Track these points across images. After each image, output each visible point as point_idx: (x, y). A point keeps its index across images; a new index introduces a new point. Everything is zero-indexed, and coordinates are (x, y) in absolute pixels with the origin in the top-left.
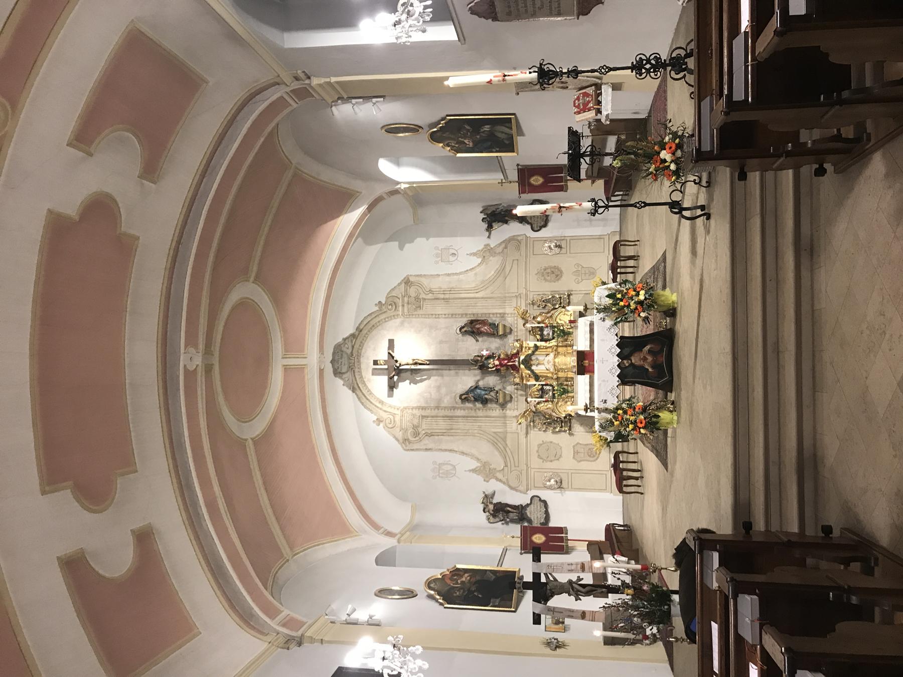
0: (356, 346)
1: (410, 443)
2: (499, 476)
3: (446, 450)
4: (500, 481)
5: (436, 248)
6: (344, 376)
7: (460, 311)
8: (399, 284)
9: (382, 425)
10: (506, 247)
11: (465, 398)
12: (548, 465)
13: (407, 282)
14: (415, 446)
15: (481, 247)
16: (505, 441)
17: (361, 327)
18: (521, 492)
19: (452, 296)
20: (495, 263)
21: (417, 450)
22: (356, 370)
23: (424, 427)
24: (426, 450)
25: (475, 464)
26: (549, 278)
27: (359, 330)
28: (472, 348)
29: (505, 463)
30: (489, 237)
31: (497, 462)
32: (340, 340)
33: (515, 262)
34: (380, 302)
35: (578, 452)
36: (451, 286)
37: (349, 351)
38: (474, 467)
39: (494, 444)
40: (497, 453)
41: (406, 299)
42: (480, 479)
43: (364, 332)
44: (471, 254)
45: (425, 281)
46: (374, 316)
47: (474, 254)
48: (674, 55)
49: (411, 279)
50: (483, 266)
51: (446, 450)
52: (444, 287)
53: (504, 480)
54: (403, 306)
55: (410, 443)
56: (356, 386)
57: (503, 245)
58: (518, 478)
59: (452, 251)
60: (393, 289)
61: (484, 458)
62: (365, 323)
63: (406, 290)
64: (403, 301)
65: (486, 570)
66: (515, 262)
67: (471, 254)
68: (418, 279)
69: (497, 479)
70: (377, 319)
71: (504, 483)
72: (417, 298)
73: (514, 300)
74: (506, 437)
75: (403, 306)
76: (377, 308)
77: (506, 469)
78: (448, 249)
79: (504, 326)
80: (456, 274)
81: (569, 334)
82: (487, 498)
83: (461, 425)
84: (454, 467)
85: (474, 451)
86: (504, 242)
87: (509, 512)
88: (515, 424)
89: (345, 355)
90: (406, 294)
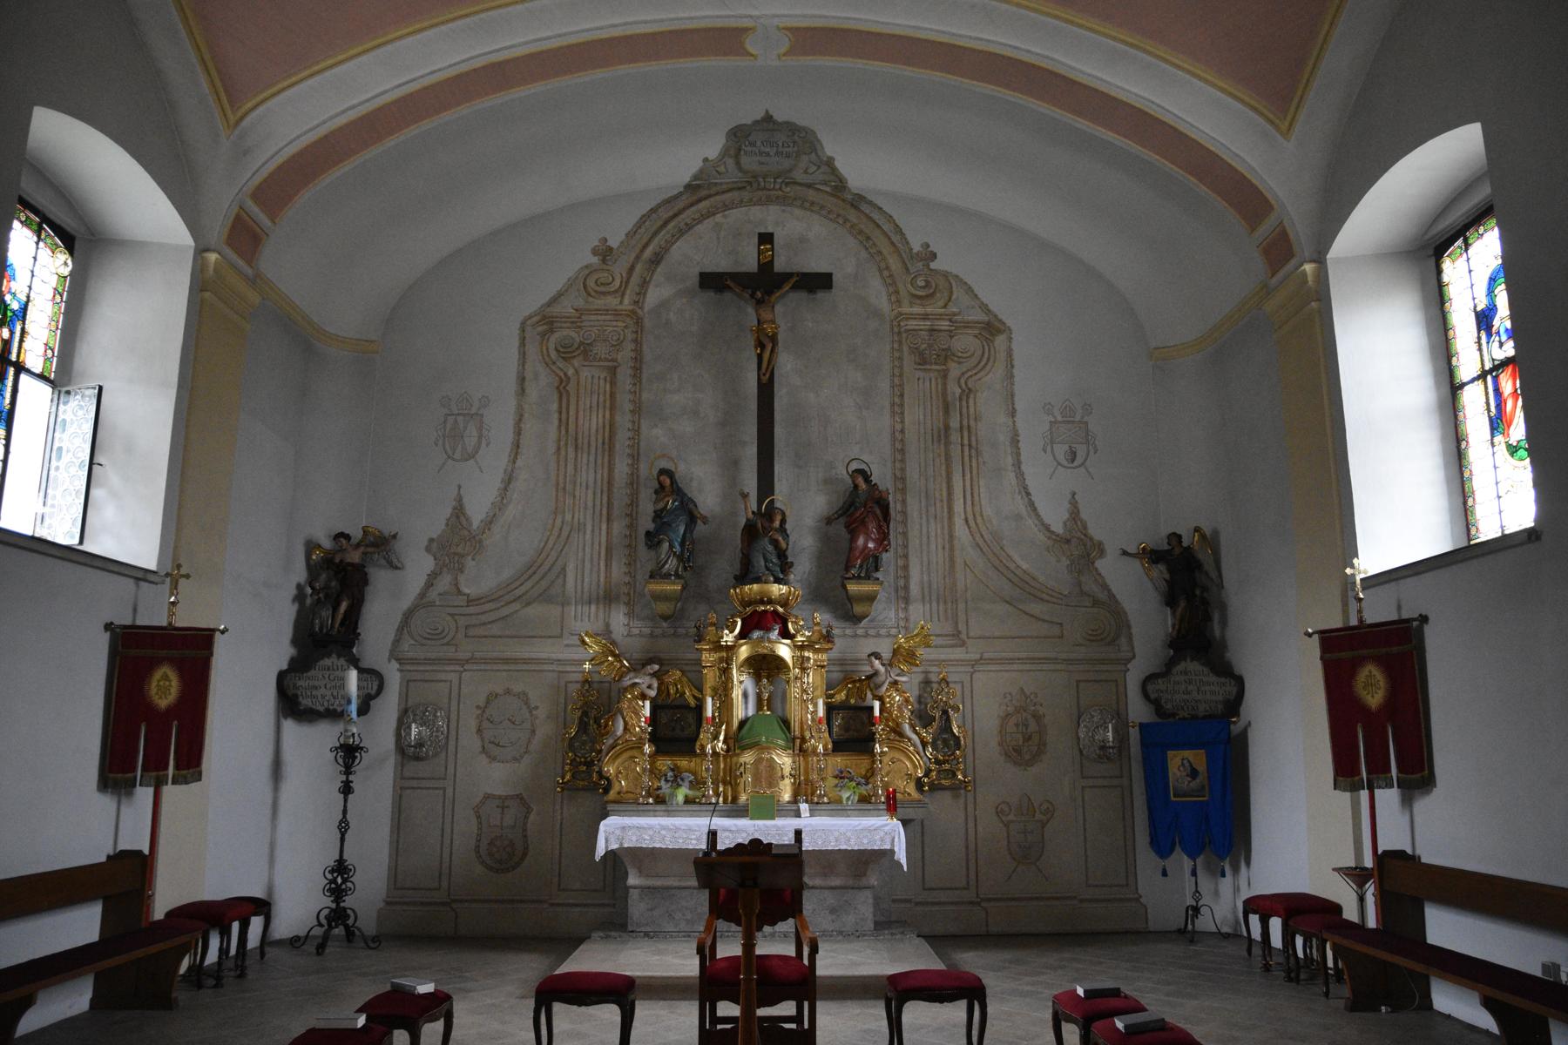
33: (1056, 630)
50: (1041, 537)
57: (1102, 596)
67: (1074, 504)
86: (1112, 596)
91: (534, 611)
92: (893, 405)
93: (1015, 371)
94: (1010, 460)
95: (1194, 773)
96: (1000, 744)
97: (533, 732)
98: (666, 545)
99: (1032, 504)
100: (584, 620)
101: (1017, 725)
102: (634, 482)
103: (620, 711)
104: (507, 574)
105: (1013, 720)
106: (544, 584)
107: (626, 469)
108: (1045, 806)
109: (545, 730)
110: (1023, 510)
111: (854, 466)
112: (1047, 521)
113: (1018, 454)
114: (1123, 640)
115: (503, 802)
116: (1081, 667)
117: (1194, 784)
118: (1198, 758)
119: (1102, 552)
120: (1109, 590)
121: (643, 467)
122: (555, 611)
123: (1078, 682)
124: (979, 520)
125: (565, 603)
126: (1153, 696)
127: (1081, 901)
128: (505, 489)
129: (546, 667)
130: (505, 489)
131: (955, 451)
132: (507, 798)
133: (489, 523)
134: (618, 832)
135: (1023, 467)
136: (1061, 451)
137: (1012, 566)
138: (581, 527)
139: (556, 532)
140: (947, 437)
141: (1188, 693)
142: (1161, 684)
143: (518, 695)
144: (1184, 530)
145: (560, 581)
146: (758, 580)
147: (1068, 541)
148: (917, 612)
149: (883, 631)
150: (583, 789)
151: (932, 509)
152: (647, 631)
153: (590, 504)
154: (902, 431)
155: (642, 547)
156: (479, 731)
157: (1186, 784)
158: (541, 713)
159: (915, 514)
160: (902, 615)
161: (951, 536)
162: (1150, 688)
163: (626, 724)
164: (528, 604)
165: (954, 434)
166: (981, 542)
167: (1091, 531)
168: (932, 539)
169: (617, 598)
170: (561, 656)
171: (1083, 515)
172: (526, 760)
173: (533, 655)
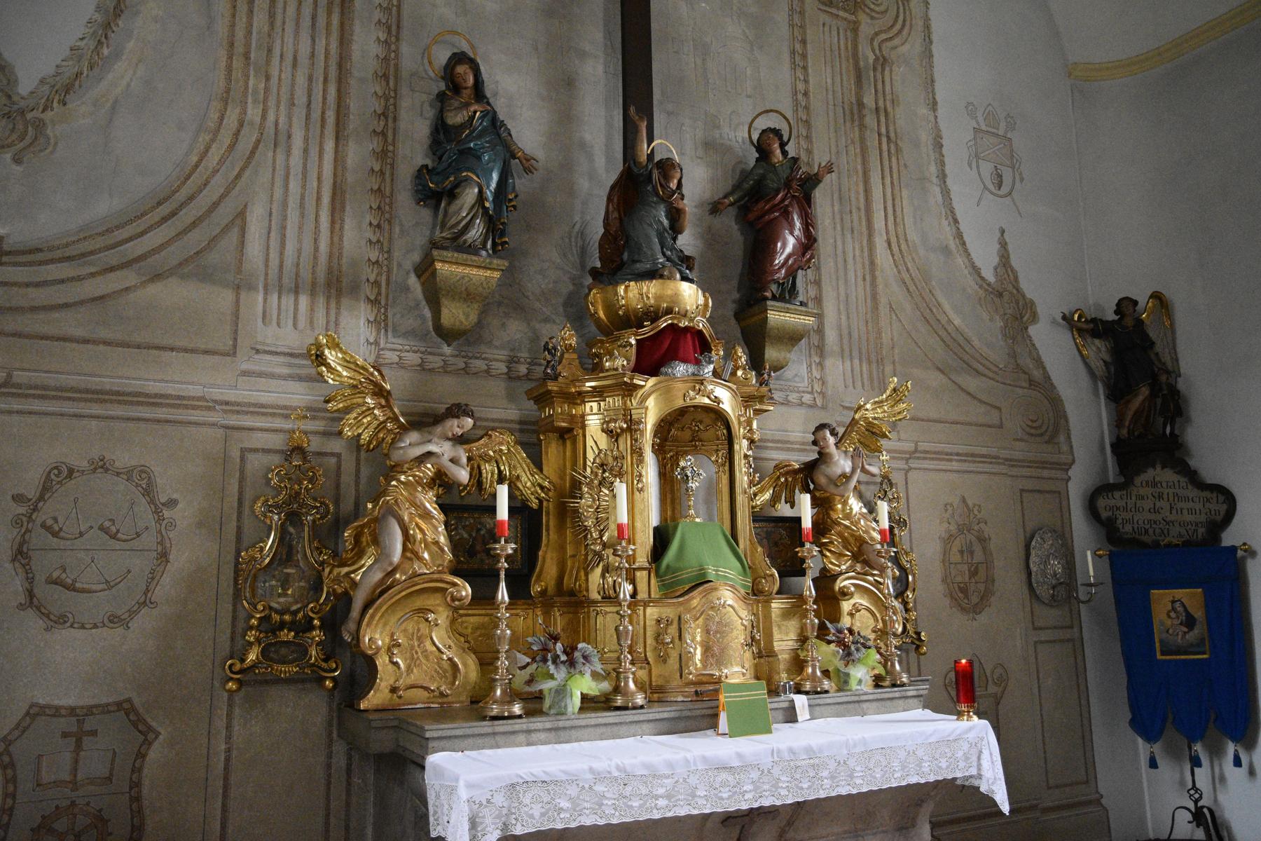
26: (956, 557)
33: (994, 417)
35: (78, 738)
44: (1003, 244)
45: (910, 47)
50: (971, 283)
57: (1037, 374)
65: (510, 508)
67: (1003, 244)
74: (206, 276)
86: (1047, 378)
91: (172, 293)
92: (793, 52)
93: (934, 48)
94: (933, 169)
95: (1190, 622)
96: (944, 580)
97: (164, 556)
98: (470, 195)
99: (959, 235)
100: (284, 324)
101: (961, 552)
102: (389, 72)
103: (391, 512)
104: (104, 207)
105: (957, 545)
106: (197, 238)
107: (375, 49)
108: (999, 671)
109: (192, 551)
110: (952, 244)
111: (763, 123)
112: (978, 263)
113: (943, 164)
114: (1062, 438)
115: (79, 724)
116: (1025, 472)
117: (1192, 636)
118: (1191, 598)
119: (1034, 318)
120: (1044, 368)
121: (409, 55)
122: (224, 298)
123: (1022, 490)
124: (903, 247)
125: (241, 286)
126: (1104, 515)
127: (1046, 810)
128: (107, 26)
129: (196, 416)
130: (107, 26)
131: (872, 141)
132: (90, 710)
133: (64, 89)
134: (499, 799)
135: (949, 181)
136: (987, 168)
137: (944, 320)
138: (281, 140)
139: (225, 138)
140: (862, 117)
141: (1156, 510)
142: (1117, 499)
143: (129, 474)
144: (1142, 296)
145: (234, 234)
146: (653, 274)
147: (1000, 295)
148: (836, 369)
149: (793, 397)
150: (289, 681)
151: (847, 218)
152: (413, 358)
153: (301, 98)
154: (806, 94)
155: (404, 198)
156: (21, 554)
157: (1181, 636)
158: (183, 515)
159: (827, 222)
160: (816, 374)
161: (872, 263)
162: (1101, 503)
163: (407, 537)
164: (156, 277)
165: (866, 112)
166: (906, 276)
167: (1024, 285)
168: (850, 260)
169: (354, 289)
170: (231, 395)
171: (1015, 262)
172: (145, 621)
173: (171, 389)
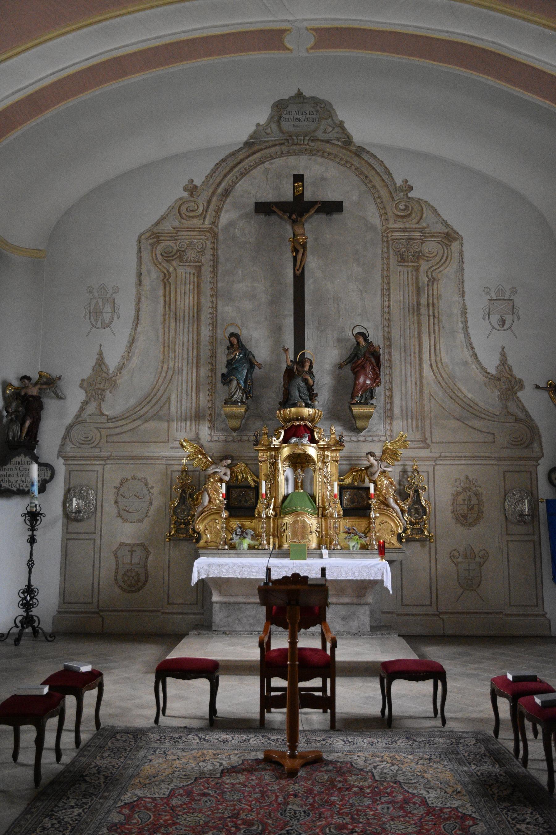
0: (328, 148)
1: (152, 245)
2: (92, 408)
3: (138, 310)
4: (82, 409)
5: (514, 291)
6: (274, 126)
7: (395, 334)
8: (445, 223)
9: (185, 194)
10: (517, 420)
11: (236, 343)
12: (110, 497)
13: (450, 237)
14: (146, 255)
15: (518, 373)
16: (152, 418)
17: (365, 156)
18: (62, 445)
19: (424, 320)
20: (488, 399)
21: (140, 258)
22: (285, 148)
23: (181, 270)
24: (139, 275)
25: (112, 361)
27: (360, 152)
28: (325, 357)
29: (115, 419)
30: (537, 387)
31: (116, 404)
32: (342, 114)
33: (490, 438)
34: (411, 188)
36: (444, 318)
37: (320, 134)
38: (107, 361)
39: (147, 399)
40: (132, 402)
41: (417, 235)
42: (86, 371)
43: (356, 162)
45: (451, 269)
46: (385, 177)
47: (504, 361)
48: (35, 618)
49: (455, 246)
50: (480, 377)
51: (138, 310)
52: (442, 305)
53: (85, 415)
54: (404, 230)
55: (152, 245)
56: (256, 148)
57: (521, 415)
58: (87, 442)
59: (509, 319)
60: (435, 211)
61: (123, 380)
62: (372, 162)
63: (432, 235)
64: (415, 230)
66: (490, 438)
68: (456, 255)
69: (84, 405)
70: (377, 182)
71: (78, 416)
72: (419, 256)
73: (418, 436)
75: (404, 230)
76: (399, 183)
77: (104, 419)
78: (514, 311)
79: (368, 417)
80: (466, 327)
81: (142, 545)
82: (50, 383)
83: (184, 338)
84: (108, 325)
85: (135, 361)
86: (528, 415)
87: (23, 424)
88: (182, 435)
89: (313, 126)
90: (426, 235)
